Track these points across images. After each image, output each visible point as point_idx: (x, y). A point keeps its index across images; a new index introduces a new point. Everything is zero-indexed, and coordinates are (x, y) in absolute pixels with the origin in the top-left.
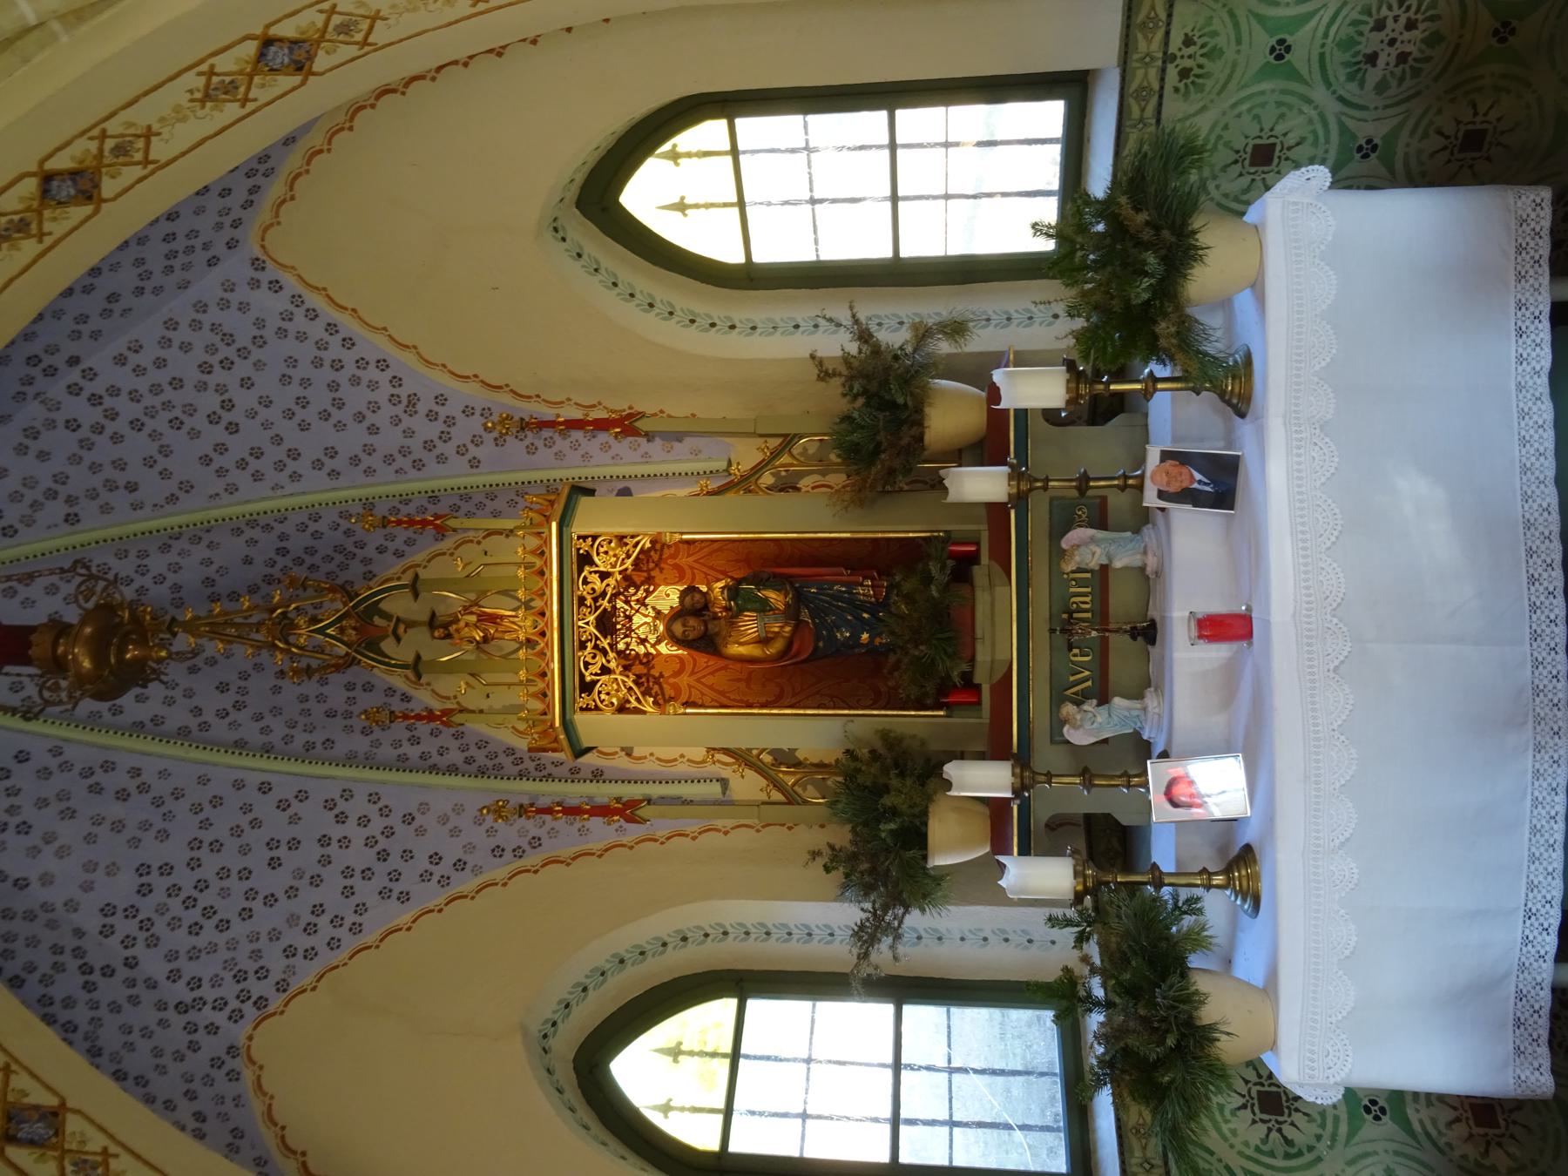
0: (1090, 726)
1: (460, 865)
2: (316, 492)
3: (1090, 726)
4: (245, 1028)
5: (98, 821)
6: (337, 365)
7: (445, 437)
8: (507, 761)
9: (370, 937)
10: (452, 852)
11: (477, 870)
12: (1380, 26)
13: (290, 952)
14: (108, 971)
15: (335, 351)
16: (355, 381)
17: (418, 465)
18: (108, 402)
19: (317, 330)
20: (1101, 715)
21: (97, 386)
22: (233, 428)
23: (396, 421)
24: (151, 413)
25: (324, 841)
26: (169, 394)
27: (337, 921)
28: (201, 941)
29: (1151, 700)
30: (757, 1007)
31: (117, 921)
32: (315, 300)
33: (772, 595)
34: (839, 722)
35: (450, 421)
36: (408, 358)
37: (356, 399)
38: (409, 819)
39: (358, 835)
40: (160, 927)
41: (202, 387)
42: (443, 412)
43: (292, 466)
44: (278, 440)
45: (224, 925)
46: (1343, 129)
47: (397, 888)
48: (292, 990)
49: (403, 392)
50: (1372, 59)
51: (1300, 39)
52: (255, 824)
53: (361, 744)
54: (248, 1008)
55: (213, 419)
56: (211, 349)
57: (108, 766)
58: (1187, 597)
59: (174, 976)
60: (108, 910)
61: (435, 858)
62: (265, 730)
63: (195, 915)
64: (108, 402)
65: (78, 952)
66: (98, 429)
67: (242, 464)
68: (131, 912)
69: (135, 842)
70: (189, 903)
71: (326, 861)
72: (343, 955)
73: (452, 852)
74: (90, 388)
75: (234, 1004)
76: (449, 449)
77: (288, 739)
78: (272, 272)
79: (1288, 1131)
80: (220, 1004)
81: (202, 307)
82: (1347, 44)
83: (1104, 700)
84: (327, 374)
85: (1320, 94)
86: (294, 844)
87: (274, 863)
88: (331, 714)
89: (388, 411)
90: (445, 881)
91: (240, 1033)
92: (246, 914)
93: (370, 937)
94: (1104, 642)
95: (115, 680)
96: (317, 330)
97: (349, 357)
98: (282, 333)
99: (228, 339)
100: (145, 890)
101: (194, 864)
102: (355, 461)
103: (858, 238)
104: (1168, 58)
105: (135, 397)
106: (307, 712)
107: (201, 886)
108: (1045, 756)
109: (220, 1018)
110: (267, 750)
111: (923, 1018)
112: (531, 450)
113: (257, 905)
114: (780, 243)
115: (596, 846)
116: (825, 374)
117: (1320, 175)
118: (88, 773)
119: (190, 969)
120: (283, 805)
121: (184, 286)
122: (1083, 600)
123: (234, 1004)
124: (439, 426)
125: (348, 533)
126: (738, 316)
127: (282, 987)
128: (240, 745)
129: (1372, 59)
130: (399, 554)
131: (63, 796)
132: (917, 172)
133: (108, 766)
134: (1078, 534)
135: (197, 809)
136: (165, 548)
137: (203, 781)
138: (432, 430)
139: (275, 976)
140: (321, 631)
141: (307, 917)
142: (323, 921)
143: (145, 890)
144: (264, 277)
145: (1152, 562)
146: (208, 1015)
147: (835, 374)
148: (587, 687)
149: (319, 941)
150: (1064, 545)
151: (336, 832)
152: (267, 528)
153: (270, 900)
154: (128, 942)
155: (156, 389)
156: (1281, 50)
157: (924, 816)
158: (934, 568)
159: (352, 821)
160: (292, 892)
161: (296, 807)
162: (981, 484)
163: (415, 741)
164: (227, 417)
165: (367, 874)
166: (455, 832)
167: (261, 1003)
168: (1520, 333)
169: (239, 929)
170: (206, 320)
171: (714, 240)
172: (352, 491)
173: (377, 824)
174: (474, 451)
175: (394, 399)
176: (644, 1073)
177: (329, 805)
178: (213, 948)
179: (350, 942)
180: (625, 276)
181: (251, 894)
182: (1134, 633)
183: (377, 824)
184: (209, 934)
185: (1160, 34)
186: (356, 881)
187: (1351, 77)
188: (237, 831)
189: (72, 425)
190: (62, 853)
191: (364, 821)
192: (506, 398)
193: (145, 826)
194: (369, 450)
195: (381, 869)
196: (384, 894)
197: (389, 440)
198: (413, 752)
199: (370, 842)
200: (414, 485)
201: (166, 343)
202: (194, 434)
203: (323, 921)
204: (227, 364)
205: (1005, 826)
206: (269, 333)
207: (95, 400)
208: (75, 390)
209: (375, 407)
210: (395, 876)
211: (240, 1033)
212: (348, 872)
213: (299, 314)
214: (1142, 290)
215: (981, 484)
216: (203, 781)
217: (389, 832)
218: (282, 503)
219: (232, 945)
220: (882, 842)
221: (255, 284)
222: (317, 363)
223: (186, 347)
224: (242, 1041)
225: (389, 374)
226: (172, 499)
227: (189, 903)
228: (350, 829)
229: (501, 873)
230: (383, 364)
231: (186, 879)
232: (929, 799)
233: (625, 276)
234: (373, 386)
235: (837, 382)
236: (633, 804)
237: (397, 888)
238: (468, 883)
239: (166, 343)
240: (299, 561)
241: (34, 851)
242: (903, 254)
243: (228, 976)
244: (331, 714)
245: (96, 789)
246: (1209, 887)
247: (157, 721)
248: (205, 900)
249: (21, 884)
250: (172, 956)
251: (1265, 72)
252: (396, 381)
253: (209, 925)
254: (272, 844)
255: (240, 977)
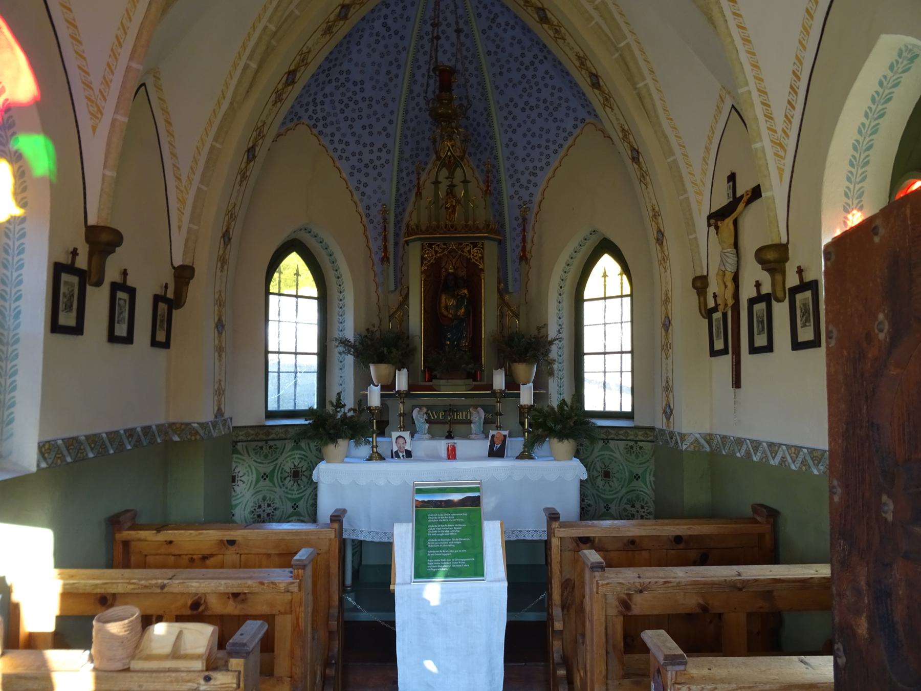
0: (419, 416)
1: (363, 194)
2: (500, 140)
3: (419, 416)
4: (307, 121)
5: (379, 65)
6: (547, 148)
7: (521, 186)
8: (401, 209)
9: (337, 163)
10: (368, 191)
11: (361, 200)
12: (642, 507)
13: (333, 135)
14: (328, 76)
15: (553, 147)
16: (542, 154)
17: (511, 176)
18: (532, 68)
19: (560, 140)
20: (422, 420)
21: (537, 64)
22: (523, 110)
23: (527, 168)
24: (528, 82)
25: (372, 144)
26: (535, 88)
27: (343, 151)
28: (337, 104)
29: (427, 436)
30: (314, 304)
31: (345, 76)
32: (570, 141)
33: (463, 310)
34: (418, 333)
35: (527, 188)
36: (550, 174)
37: (535, 154)
38: (380, 174)
39: (373, 157)
40: (342, 90)
41: (538, 99)
42: (531, 186)
43: (510, 130)
44: (519, 126)
45: (342, 111)
46: (613, 500)
47: (355, 172)
48: (320, 137)
49: (538, 171)
50: (633, 506)
51: (640, 483)
52: (378, 120)
53: (407, 155)
54: (313, 122)
55: (527, 103)
56: (552, 103)
57: (399, 67)
58: (461, 445)
59: (325, 96)
60: (348, 72)
61: (366, 185)
62: (412, 120)
63: (346, 101)
64: (532, 68)
65: (335, 66)
66: (522, 64)
67: (510, 113)
68: (348, 80)
69: (371, 79)
70: (350, 99)
71: (365, 145)
72: (331, 153)
73: (368, 191)
74: (537, 61)
75: (315, 117)
76: (517, 188)
77: (408, 128)
78: (580, 126)
79: (288, 479)
80: (315, 112)
81: (567, 100)
82: (638, 498)
83: (427, 421)
84: (544, 144)
85: (624, 491)
86: (371, 134)
87: (364, 127)
88: (418, 143)
89: (531, 165)
90: (357, 189)
91: (305, 120)
92: (346, 119)
93: (337, 163)
94: (446, 423)
95: (433, 113)
96: (560, 140)
97: (550, 152)
98: (558, 128)
99: (556, 109)
100: (355, 83)
101: (364, 99)
102: (512, 153)
103: (591, 342)
104: (636, 442)
105: (534, 76)
106: (418, 134)
107: (356, 102)
108: (409, 402)
109: (310, 112)
110: (405, 122)
111: (313, 361)
112: (517, 219)
113: (349, 122)
114: (591, 312)
115: (370, 244)
116: (539, 329)
117: (585, 477)
118: (397, 60)
119: (327, 101)
120: (385, 129)
121: (574, 95)
122: (461, 416)
123: (315, 117)
124: (526, 184)
125: (486, 149)
126: (565, 296)
127: (321, 133)
128: (406, 112)
129: (633, 506)
130: (478, 166)
131: (388, 53)
132: (613, 361)
133: (399, 67)
134: (483, 414)
135: (383, 98)
136: (479, 84)
137: (393, 100)
138: (524, 181)
139: (325, 131)
140: (449, 150)
141: (345, 140)
142: (343, 146)
143: (355, 83)
144: (578, 123)
145: (473, 436)
146: (311, 108)
147: (539, 332)
148: (430, 246)
149: (336, 145)
150: (479, 409)
151: (375, 149)
152: (487, 120)
153: (351, 127)
154: (337, 79)
155: (537, 84)
156: (637, 477)
157: (388, 363)
158: (471, 366)
159: (379, 154)
160: (354, 134)
161: (384, 134)
162: (499, 381)
163: (408, 175)
164: (527, 108)
165: (360, 160)
166: (375, 192)
167: (315, 126)
168: (536, 531)
169: (341, 117)
170: (562, 102)
171: (592, 288)
172: (501, 152)
173: (377, 163)
174: (516, 197)
175: (535, 168)
176: (293, 262)
177: (385, 146)
178: (334, 108)
179: (335, 156)
180: (579, 255)
181: (353, 120)
182: (449, 432)
183: (377, 163)
184: (339, 106)
185: (643, 438)
186: (357, 157)
187: (628, 500)
188: (375, 113)
189: (523, 55)
190: (369, 55)
191: (379, 158)
192: (536, 209)
193: (377, 82)
194: (516, 159)
195: (362, 165)
196: (353, 167)
197: (521, 166)
198: (404, 174)
199: (371, 161)
200: (503, 175)
201: (554, 87)
202: (521, 96)
203: (343, 146)
204: (547, 109)
205: (388, 387)
206: (558, 124)
207: (532, 63)
208: (535, 56)
209: (532, 161)
210: (359, 171)
211: (305, 120)
212: (361, 153)
213: (566, 134)
214: (551, 424)
215: (499, 381)
216: (393, 100)
217: (375, 168)
218: (496, 128)
219: (335, 115)
220: (376, 347)
221: (576, 119)
222: (548, 141)
223: (552, 95)
224: (302, 121)
225: (544, 166)
226: (497, 87)
227: (350, 99)
228: (376, 154)
229: (360, 209)
230: (548, 164)
231: (358, 97)
232: (393, 364)
233: (579, 255)
234: (540, 160)
235: (536, 333)
236: (388, 260)
237: (355, 172)
238: (357, 197)
239: (554, 87)
240: (475, 130)
241: (369, 46)
242: (316, 351)
243: (324, 114)
244: (418, 143)
245: (391, 63)
246: (372, 447)
247: (415, 82)
248: (351, 104)
249: (358, 44)
250: (332, 95)
251: (631, 472)
252: (542, 169)
253: (342, 106)
254: (371, 126)
255: (324, 118)
